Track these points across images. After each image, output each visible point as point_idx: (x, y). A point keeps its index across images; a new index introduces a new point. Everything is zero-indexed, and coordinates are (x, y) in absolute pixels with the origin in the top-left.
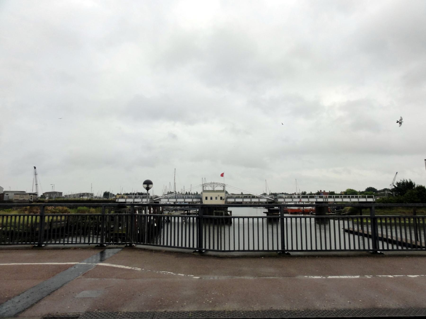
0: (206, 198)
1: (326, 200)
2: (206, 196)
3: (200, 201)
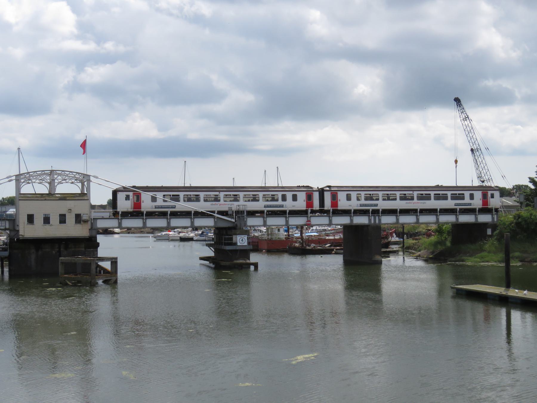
0: (31, 219)
1: (377, 222)
2: (31, 213)
3: (7, 227)
